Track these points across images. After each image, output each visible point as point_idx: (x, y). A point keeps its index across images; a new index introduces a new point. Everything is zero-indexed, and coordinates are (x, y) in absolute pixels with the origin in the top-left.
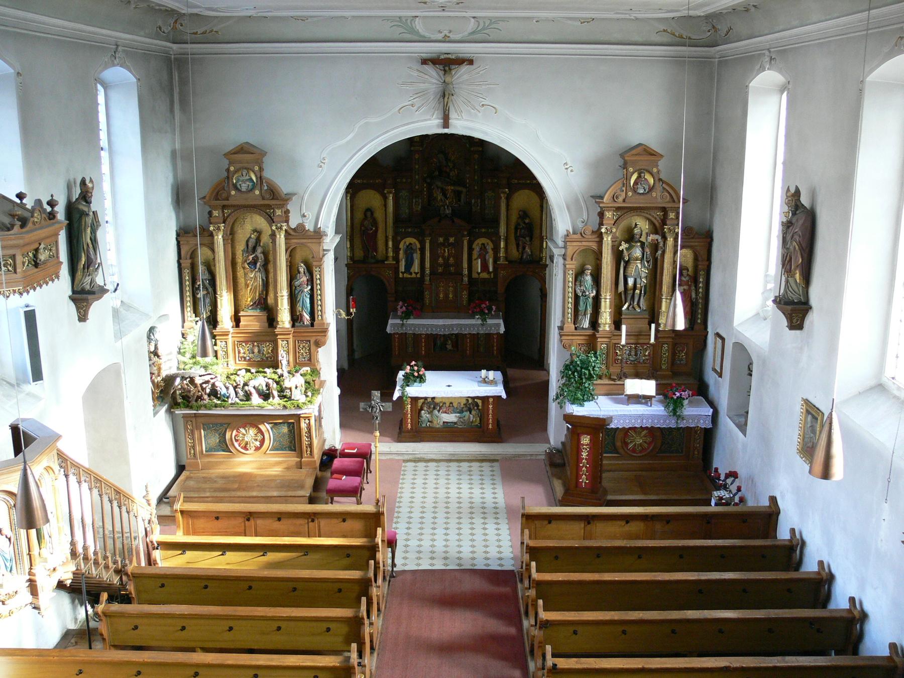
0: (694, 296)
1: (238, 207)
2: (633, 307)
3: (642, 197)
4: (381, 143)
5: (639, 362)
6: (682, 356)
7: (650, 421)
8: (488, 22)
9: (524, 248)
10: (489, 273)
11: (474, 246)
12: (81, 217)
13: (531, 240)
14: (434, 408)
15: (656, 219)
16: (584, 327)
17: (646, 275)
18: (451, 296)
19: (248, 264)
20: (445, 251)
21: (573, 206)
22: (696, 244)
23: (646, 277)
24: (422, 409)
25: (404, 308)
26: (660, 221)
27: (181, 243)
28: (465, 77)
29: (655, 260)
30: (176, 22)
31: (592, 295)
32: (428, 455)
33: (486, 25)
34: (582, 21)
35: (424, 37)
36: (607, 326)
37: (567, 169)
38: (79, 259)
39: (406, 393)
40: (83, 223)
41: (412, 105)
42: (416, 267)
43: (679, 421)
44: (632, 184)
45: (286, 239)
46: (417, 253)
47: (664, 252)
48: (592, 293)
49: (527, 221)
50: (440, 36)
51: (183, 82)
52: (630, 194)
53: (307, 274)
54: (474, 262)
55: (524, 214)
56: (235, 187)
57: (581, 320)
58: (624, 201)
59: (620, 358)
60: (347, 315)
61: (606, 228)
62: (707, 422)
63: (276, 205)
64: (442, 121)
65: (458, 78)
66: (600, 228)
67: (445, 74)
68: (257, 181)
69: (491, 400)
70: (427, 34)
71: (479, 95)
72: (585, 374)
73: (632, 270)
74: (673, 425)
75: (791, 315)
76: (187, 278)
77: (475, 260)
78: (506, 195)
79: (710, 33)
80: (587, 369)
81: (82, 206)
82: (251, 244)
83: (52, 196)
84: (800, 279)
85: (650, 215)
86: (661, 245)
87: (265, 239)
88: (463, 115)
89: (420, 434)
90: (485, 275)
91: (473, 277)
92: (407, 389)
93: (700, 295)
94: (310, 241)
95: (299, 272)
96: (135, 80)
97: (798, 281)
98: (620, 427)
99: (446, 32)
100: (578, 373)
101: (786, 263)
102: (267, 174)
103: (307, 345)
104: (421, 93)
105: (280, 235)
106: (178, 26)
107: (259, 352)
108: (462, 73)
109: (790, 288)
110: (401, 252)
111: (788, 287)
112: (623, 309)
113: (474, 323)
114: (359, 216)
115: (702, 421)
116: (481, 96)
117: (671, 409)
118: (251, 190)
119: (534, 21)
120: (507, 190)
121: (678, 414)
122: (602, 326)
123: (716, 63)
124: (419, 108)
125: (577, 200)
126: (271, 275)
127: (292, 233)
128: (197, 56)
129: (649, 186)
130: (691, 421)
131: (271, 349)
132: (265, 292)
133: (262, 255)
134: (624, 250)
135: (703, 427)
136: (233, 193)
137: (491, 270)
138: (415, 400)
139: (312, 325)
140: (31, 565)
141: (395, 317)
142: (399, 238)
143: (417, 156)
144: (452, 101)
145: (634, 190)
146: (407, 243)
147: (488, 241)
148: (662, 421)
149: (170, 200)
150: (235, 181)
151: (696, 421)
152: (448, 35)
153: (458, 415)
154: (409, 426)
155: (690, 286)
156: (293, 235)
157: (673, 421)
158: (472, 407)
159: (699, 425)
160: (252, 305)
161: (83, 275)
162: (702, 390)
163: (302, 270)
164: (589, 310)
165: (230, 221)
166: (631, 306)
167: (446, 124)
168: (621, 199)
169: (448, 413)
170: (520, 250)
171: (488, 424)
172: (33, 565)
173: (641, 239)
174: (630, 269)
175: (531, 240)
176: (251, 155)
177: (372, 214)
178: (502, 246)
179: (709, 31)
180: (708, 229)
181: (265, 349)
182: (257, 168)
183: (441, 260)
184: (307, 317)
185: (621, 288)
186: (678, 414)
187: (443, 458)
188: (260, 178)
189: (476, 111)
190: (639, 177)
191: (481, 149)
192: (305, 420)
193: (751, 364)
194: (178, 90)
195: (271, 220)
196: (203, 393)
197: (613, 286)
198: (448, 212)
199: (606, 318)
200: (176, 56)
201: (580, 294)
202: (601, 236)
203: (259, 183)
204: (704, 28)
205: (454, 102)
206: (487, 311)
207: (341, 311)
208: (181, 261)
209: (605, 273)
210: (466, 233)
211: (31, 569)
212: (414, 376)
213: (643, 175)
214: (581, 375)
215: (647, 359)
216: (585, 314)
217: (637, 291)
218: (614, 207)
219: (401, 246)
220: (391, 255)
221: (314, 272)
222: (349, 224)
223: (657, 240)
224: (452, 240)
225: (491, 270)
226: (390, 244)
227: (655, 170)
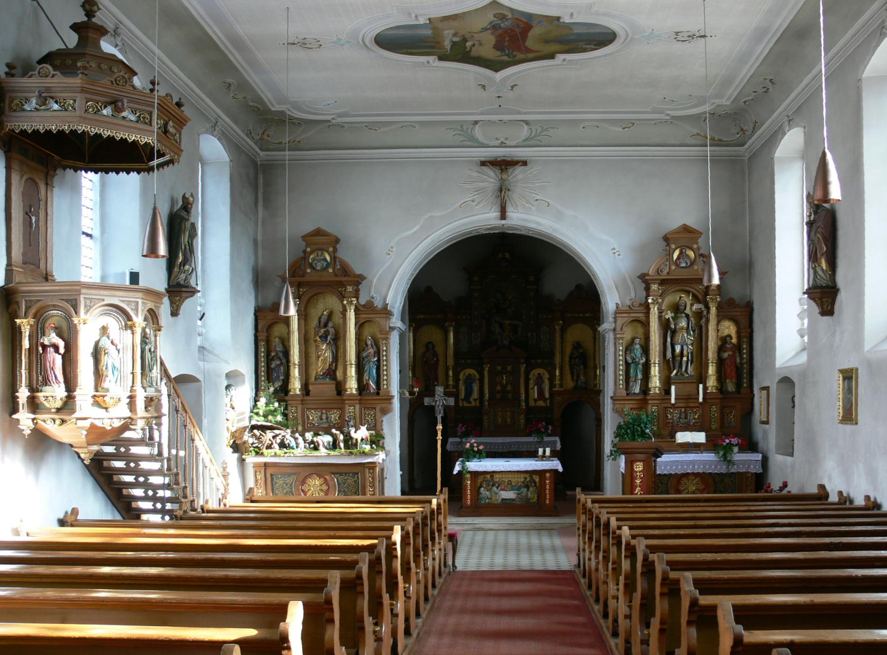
0: (738, 360)
1: (310, 284)
2: (681, 374)
3: (685, 270)
4: (444, 233)
5: (690, 425)
6: (731, 419)
7: (702, 466)
8: (539, 130)
9: (578, 376)
10: (545, 400)
11: (531, 376)
12: (181, 222)
13: (585, 367)
14: (493, 485)
15: (698, 291)
16: (635, 392)
17: (692, 342)
18: (509, 420)
19: (320, 337)
20: (503, 378)
21: (621, 285)
22: (739, 313)
23: (692, 344)
24: (481, 487)
25: (464, 428)
26: (703, 294)
27: (259, 317)
28: (520, 176)
29: (701, 327)
30: (263, 133)
31: (642, 362)
32: (488, 525)
33: (538, 132)
34: (624, 126)
35: (483, 144)
36: (657, 389)
37: (614, 253)
38: (177, 257)
39: (466, 467)
40: (183, 226)
41: (473, 201)
42: (475, 395)
43: (730, 467)
44: (674, 260)
45: (355, 314)
46: (476, 383)
47: (708, 321)
48: (642, 360)
49: (581, 351)
50: (498, 143)
51: (267, 184)
52: (673, 267)
53: (375, 347)
54: (531, 391)
55: (577, 345)
56: (311, 266)
57: (632, 386)
58: (668, 273)
59: (671, 421)
60: (410, 395)
61: (652, 299)
62: (757, 467)
63: (348, 281)
64: (499, 214)
65: (513, 178)
66: (647, 299)
67: (502, 172)
68: (331, 261)
69: (548, 475)
70: (486, 142)
71: (532, 191)
72: (637, 431)
73: (679, 338)
74: (724, 471)
75: (821, 299)
76: (263, 350)
77: (532, 389)
78: (560, 327)
79: (739, 135)
80: (639, 425)
81: (184, 214)
82: (323, 320)
83: (180, 99)
84: (826, 266)
85: (693, 288)
86: (705, 313)
87: (337, 318)
88: (518, 208)
89: (480, 509)
90: (541, 403)
91: (531, 405)
92: (467, 463)
93: (745, 361)
94: (378, 316)
95: (367, 345)
96: (229, 160)
97: (824, 268)
98: (673, 473)
99: (503, 140)
100: (630, 430)
101: (813, 257)
102: (339, 255)
103: (372, 412)
104: (480, 191)
105: (350, 309)
106: (265, 137)
107: (327, 418)
108: (518, 172)
109: (818, 277)
110: (461, 382)
111: (817, 277)
112: (672, 375)
113: (531, 440)
114: (422, 350)
115: (752, 466)
116: (534, 192)
117: (721, 455)
118: (325, 269)
119: (581, 127)
120: (561, 322)
121: (728, 459)
122: (652, 389)
123: (747, 161)
124: (478, 203)
125: (624, 280)
126: (341, 350)
127: (361, 308)
128: (279, 162)
129: (691, 261)
130: (741, 466)
131: (338, 416)
132: (334, 364)
133: (332, 329)
134: (671, 319)
135: (754, 472)
136: (309, 271)
137: (547, 396)
138: (475, 474)
139: (378, 394)
140: (133, 383)
141: (455, 436)
142: (459, 369)
143: (476, 294)
144: (508, 196)
145: (677, 265)
146: (467, 374)
147: (544, 371)
148: (713, 467)
149: (251, 278)
150: (310, 261)
151: (746, 466)
152: (504, 141)
153: (516, 492)
154: (469, 502)
155: (734, 353)
156: (362, 311)
157: (724, 467)
158: (529, 485)
159: (749, 471)
160: (322, 375)
161: (179, 271)
162: (750, 445)
163: (369, 343)
164: (640, 376)
165: (305, 298)
166: (679, 373)
167: (503, 216)
168: (665, 272)
169: (507, 491)
170: (575, 377)
171: (545, 499)
172: (135, 383)
173: (685, 311)
174: (677, 337)
175: (585, 367)
176: (327, 238)
177: (434, 347)
178: (557, 374)
179: (738, 134)
180: (748, 300)
181: (333, 416)
182: (331, 249)
183: (499, 388)
184: (373, 385)
185: (669, 355)
186: (728, 459)
187: (502, 528)
188: (334, 258)
189: (530, 205)
190: (681, 253)
191: (536, 287)
192: (369, 469)
193: (794, 397)
194: (262, 191)
195: (342, 297)
196: (274, 442)
197: (662, 354)
198: (506, 342)
199: (655, 382)
200: (262, 162)
201: (630, 361)
202: (647, 307)
203: (333, 263)
204: (733, 131)
205: (510, 198)
206: (543, 430)
207: (405, 390)
208: (258, 334)
209: (653, 340)
210: (523, 361)
211: (133, 386)
212: (474, 451)
213: (684, 250)
214: (634, 432)
215: (697, 422)
216: (635, 381)
217: (685, 359)
218: (659, 279)
219: (461, 376)
220: (451, 383)
221: (381, 344)
222: (412, 354)
223: (700, 309)
224: (509, 368)
225: (547, 396)
226: (451, 373)
227: (695, 246)
